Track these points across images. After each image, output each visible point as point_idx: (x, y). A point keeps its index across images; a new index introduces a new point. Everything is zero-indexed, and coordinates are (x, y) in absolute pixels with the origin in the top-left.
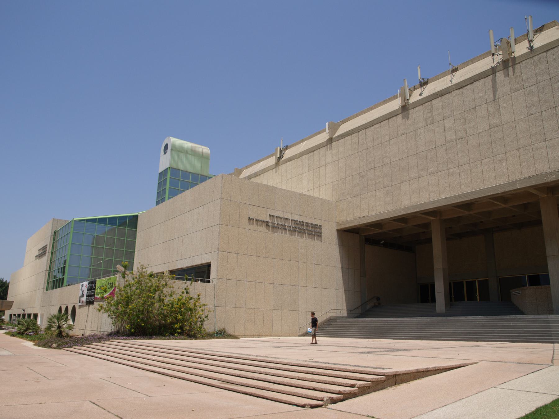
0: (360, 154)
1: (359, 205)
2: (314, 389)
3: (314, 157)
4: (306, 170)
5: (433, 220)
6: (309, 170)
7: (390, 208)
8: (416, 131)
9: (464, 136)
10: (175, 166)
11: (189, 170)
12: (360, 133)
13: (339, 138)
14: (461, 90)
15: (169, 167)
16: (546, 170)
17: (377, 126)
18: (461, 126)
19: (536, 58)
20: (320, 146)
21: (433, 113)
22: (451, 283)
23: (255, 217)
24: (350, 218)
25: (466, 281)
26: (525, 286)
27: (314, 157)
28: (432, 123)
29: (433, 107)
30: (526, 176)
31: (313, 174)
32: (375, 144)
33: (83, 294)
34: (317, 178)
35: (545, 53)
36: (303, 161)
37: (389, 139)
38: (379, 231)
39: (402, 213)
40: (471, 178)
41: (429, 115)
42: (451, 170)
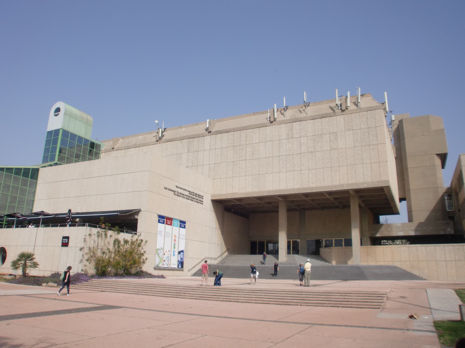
0: (235, 148)
1: (231, 184)
2: (379, 297)
3: (193, 143)
4: (186, 151)
5: (280, 200)
6: (188, 152)
7: (256, 190)
8: (280, 140)
9: (313, 151)
10: (66, 129)
11: (76, 133)
12: (236, 133)
13: (217, 133)
14: (313, 120)
15: (61, 129)
16: (362, 181)
17: (250, 131)
18: (312, 144)
19: (361, 114)
20: (200, 135)
21: (293, 131)
22: (290, 241)
23: (168, 187)
24: (223, 192)
25: (292, 241)
26: (333, 246)
27: (193, 143)
28: (292, 138)
29: (293, 127)
30: (350, 182)
31: (192, 155)
32: (247, 143)
33: (95, 240)
34: (195, 159)
35: (366, 112)
36: (183, 144)
37: (259, 142)
38: (239, 203)
39: (266, 195)
40: (316, 178)
41: (290, 132)
42: (303, 172)
